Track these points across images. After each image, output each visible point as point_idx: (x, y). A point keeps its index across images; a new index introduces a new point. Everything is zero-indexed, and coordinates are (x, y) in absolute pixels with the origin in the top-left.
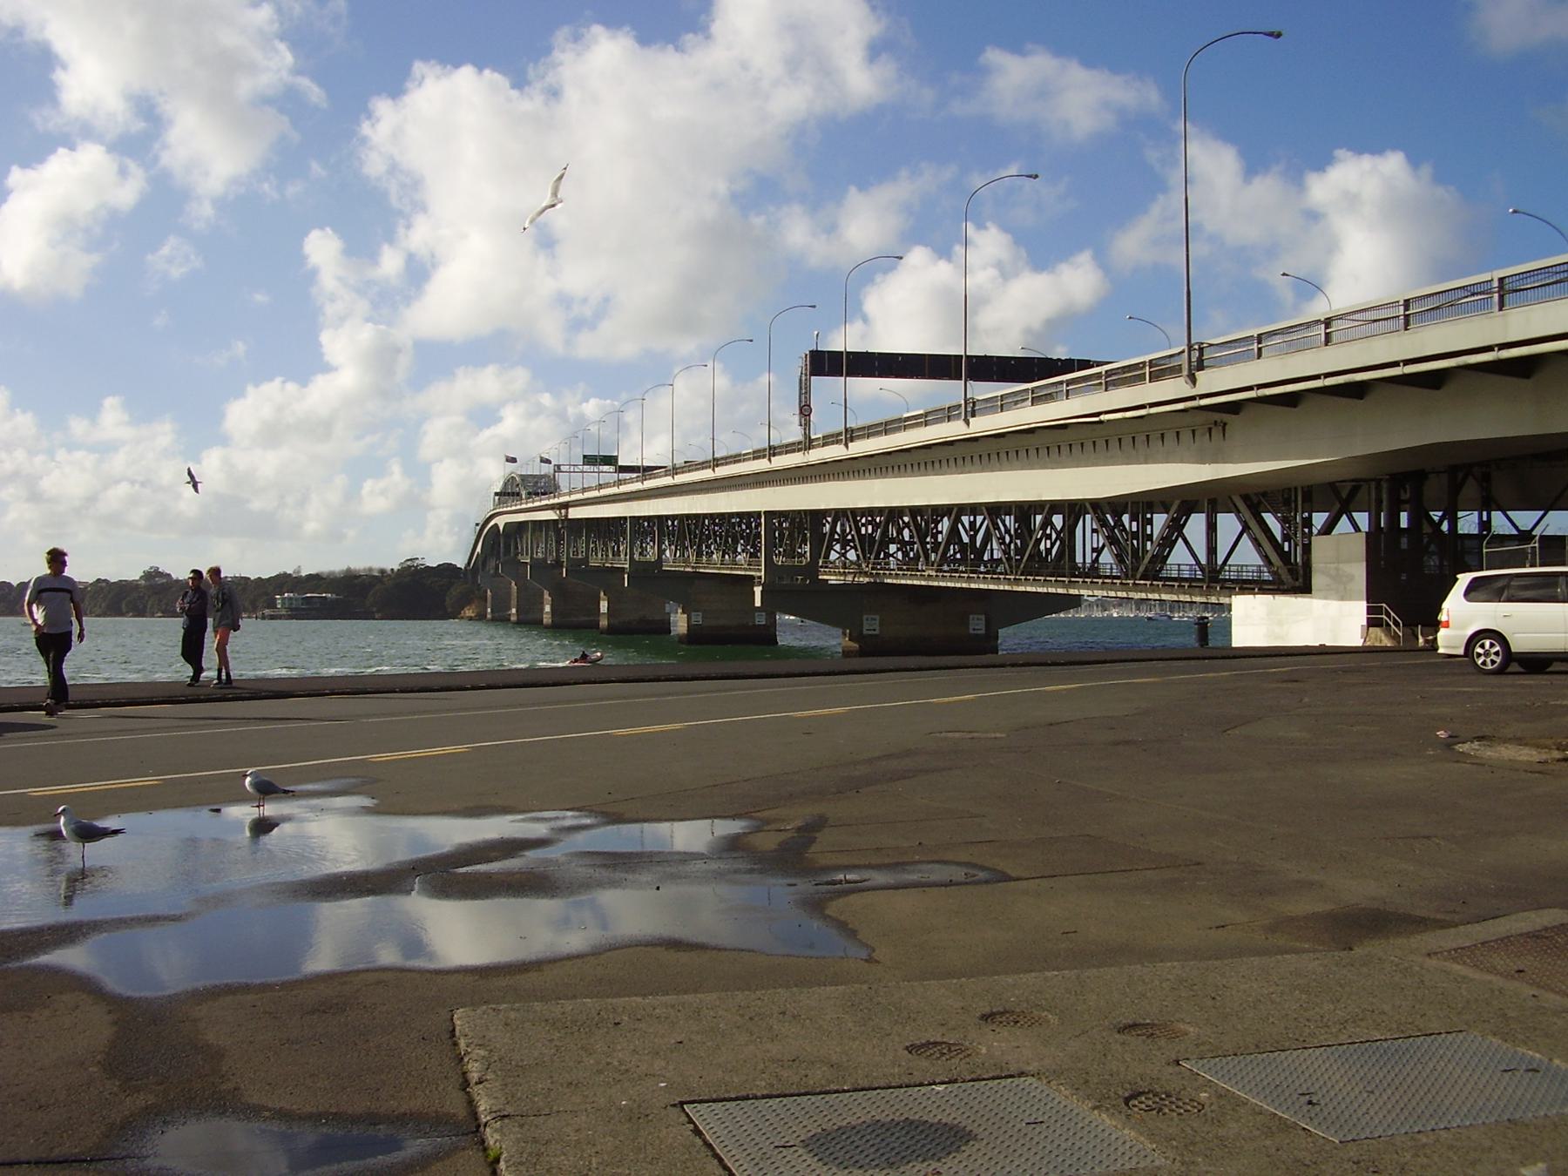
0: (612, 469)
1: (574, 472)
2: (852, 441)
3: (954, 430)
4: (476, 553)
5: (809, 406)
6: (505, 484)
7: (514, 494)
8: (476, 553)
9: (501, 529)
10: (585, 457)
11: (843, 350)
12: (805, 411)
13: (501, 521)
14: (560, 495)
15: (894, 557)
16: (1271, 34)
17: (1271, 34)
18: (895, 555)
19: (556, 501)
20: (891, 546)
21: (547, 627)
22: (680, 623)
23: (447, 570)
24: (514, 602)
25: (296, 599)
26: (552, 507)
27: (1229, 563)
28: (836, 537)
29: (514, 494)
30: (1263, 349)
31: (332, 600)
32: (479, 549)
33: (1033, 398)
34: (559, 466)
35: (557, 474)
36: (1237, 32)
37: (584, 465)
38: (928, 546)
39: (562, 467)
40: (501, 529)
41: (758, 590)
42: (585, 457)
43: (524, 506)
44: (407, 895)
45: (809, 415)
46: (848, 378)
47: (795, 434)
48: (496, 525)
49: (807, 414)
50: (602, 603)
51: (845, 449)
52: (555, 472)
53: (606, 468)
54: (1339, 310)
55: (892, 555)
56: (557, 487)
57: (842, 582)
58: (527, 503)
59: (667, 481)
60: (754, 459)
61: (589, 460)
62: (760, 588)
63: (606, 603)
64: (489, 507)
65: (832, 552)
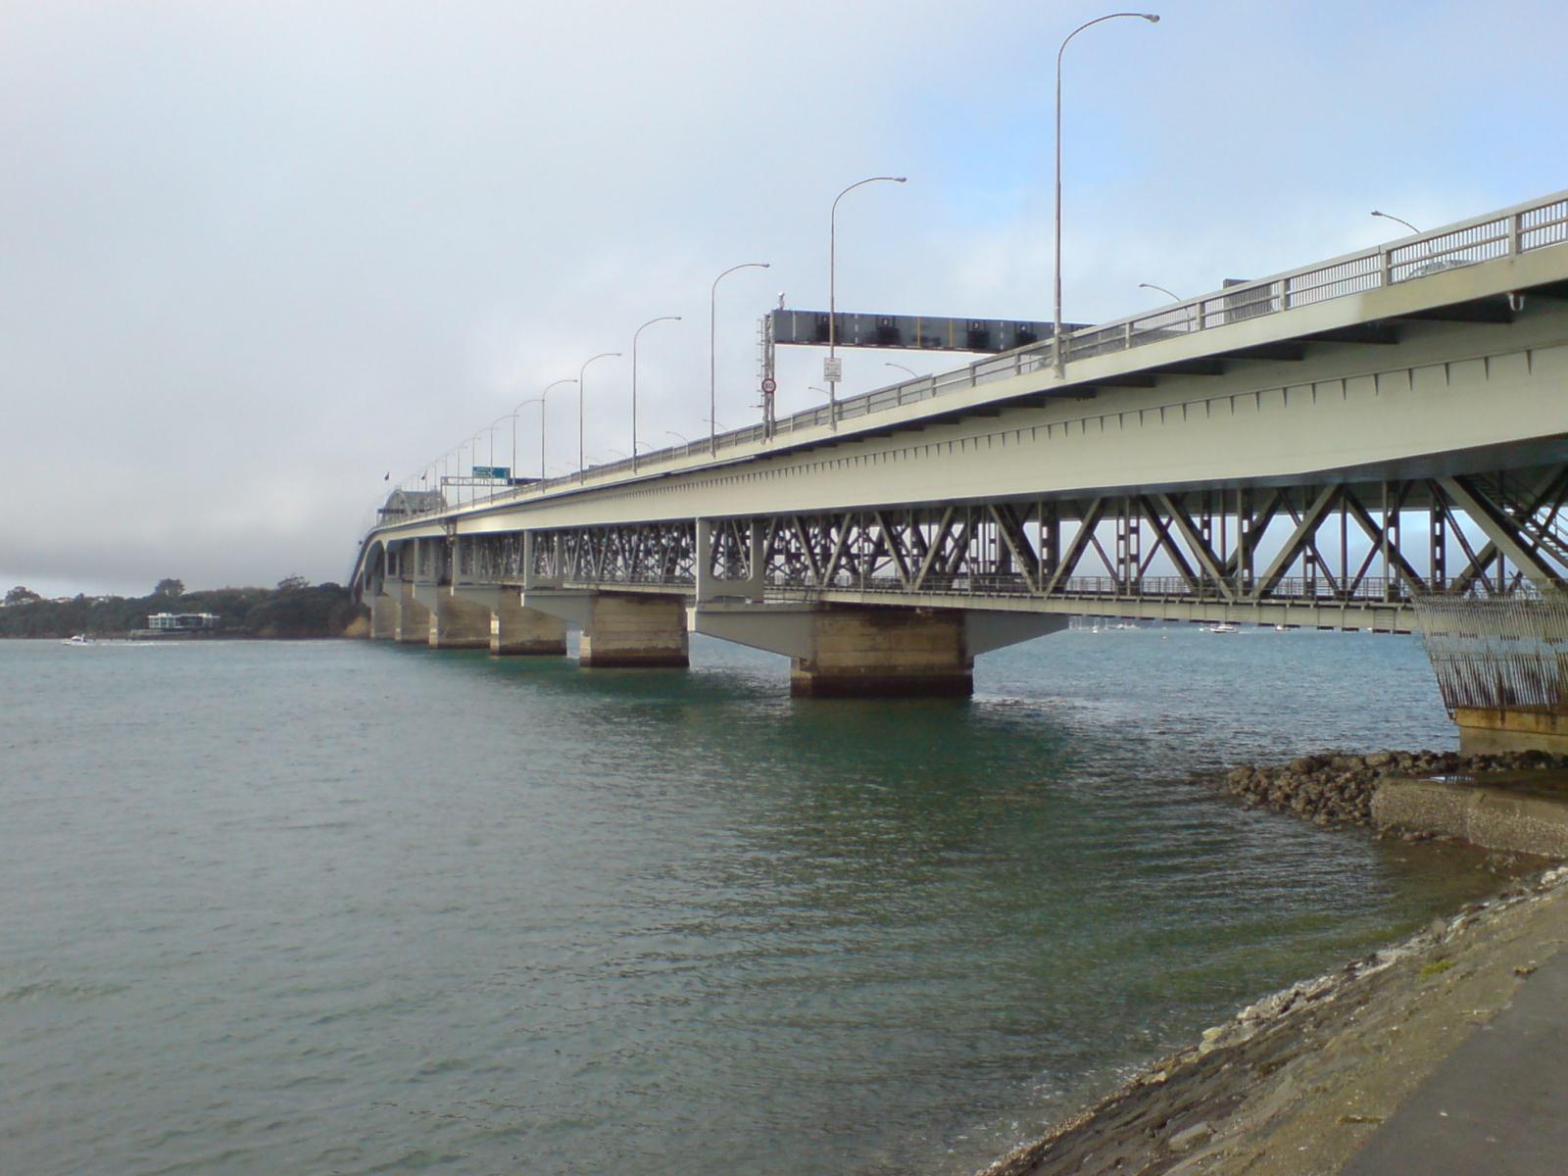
0: (504, 481)
1: (463, 485)
2: (841, 419)
3: (511, 501)
4: (359, 573)
5: (772, 380)
6: (389, 502)
7: (397, 511)
8: (359, 573)
9: (385, 547)
10: (475, 469)
11: (829, 310)
12: (769, 390)
13: (386, 540)
14: (447, 511)
15: (781, 571)
16: (1149, 17)
17: (1149, 17)
18: (783, 568)
19: (443, 515)
20: (776, 557)
21: (397, 642)
22: (581, 646)
23: (330, 589)
24: (399, 621)
25: (171, 619)
26: (439, 521)
27: (1366, 576)
28: (721, 549)
29: (397, 511)
30: (1292, 296)
31: (208, 620)
32: (362, 568)
33: (755, 436)
34: (446, 479)
35: (444, 487)
36: (1111, 14)
37: (473, 478)
38: (818, 558)
39: (449, 480)
40: (385, 547)
41: (691, 613)
42: (475, 469)
43: (408, 522)
44: (172, 585)
45: (772, 392)
46: (836, 348)
47: (757, 418)
48: (379, 543)
49: (769, 390)
50: (493, 623)
51: (712, 457)
52: (442, 485)
53: (497, 481)
54: (1103, 325)
55: (779, 568)
56: (444, 503)
57: (782, 601)
58: (412, 519)
59: (538, 494)
60: (689, 455)
61: (481, 472)
62: (695, 609)
63: (497, 623)
64: (374, 520)
65: (717, 565)
